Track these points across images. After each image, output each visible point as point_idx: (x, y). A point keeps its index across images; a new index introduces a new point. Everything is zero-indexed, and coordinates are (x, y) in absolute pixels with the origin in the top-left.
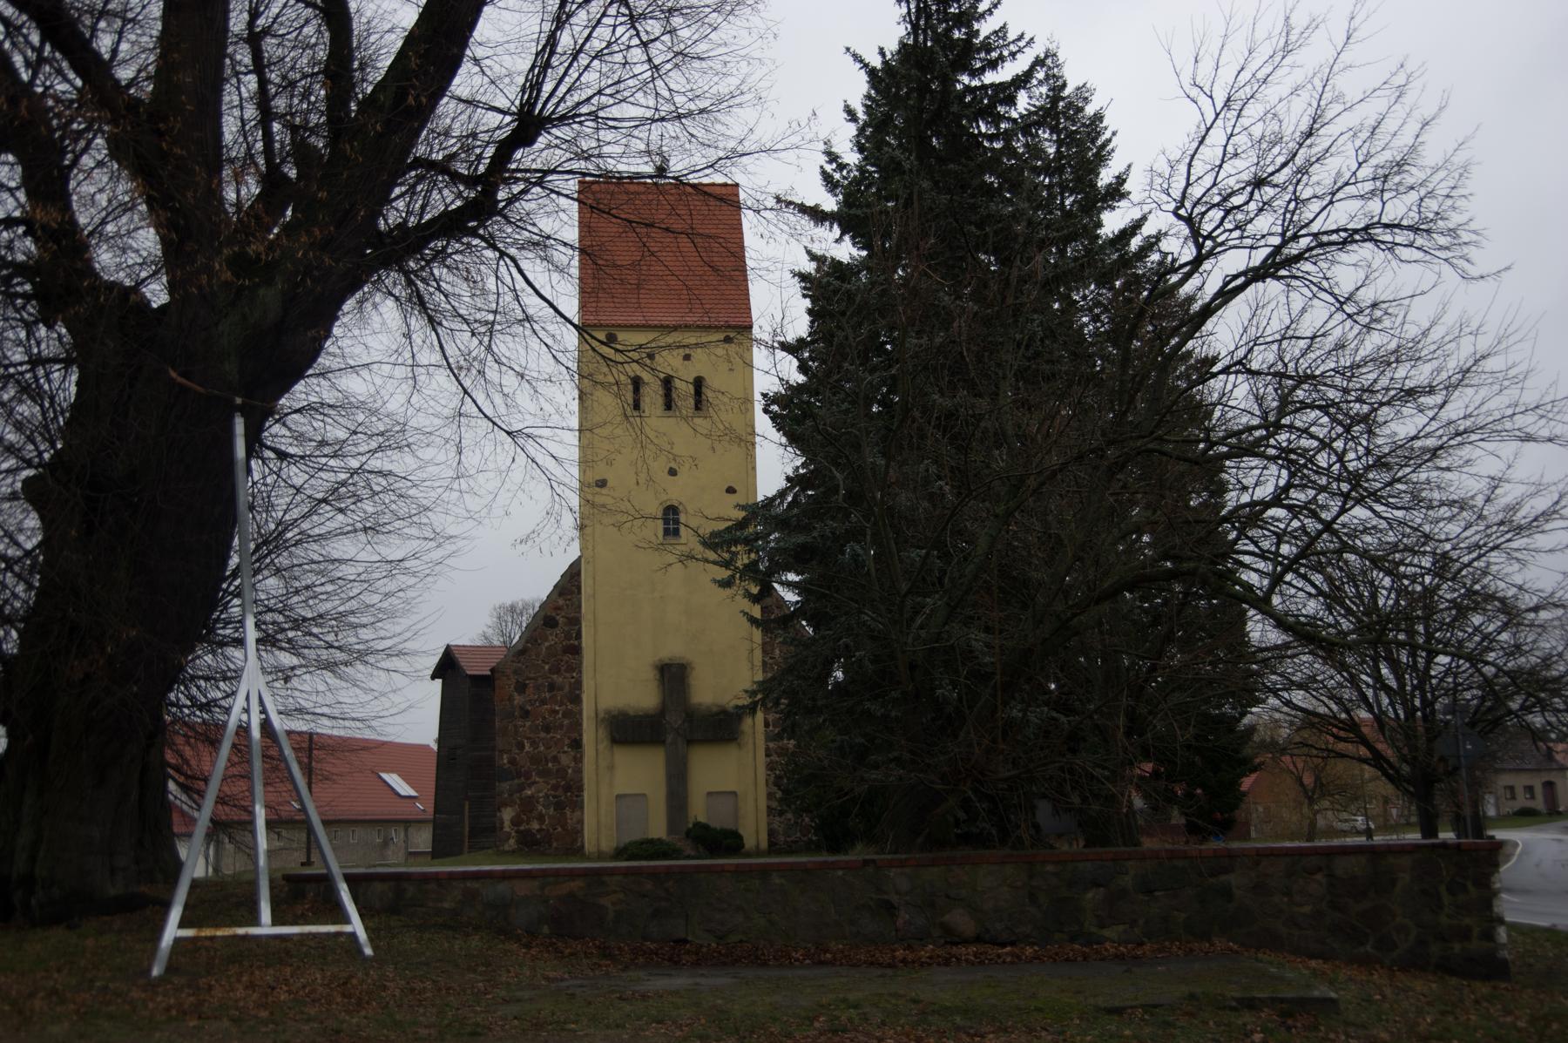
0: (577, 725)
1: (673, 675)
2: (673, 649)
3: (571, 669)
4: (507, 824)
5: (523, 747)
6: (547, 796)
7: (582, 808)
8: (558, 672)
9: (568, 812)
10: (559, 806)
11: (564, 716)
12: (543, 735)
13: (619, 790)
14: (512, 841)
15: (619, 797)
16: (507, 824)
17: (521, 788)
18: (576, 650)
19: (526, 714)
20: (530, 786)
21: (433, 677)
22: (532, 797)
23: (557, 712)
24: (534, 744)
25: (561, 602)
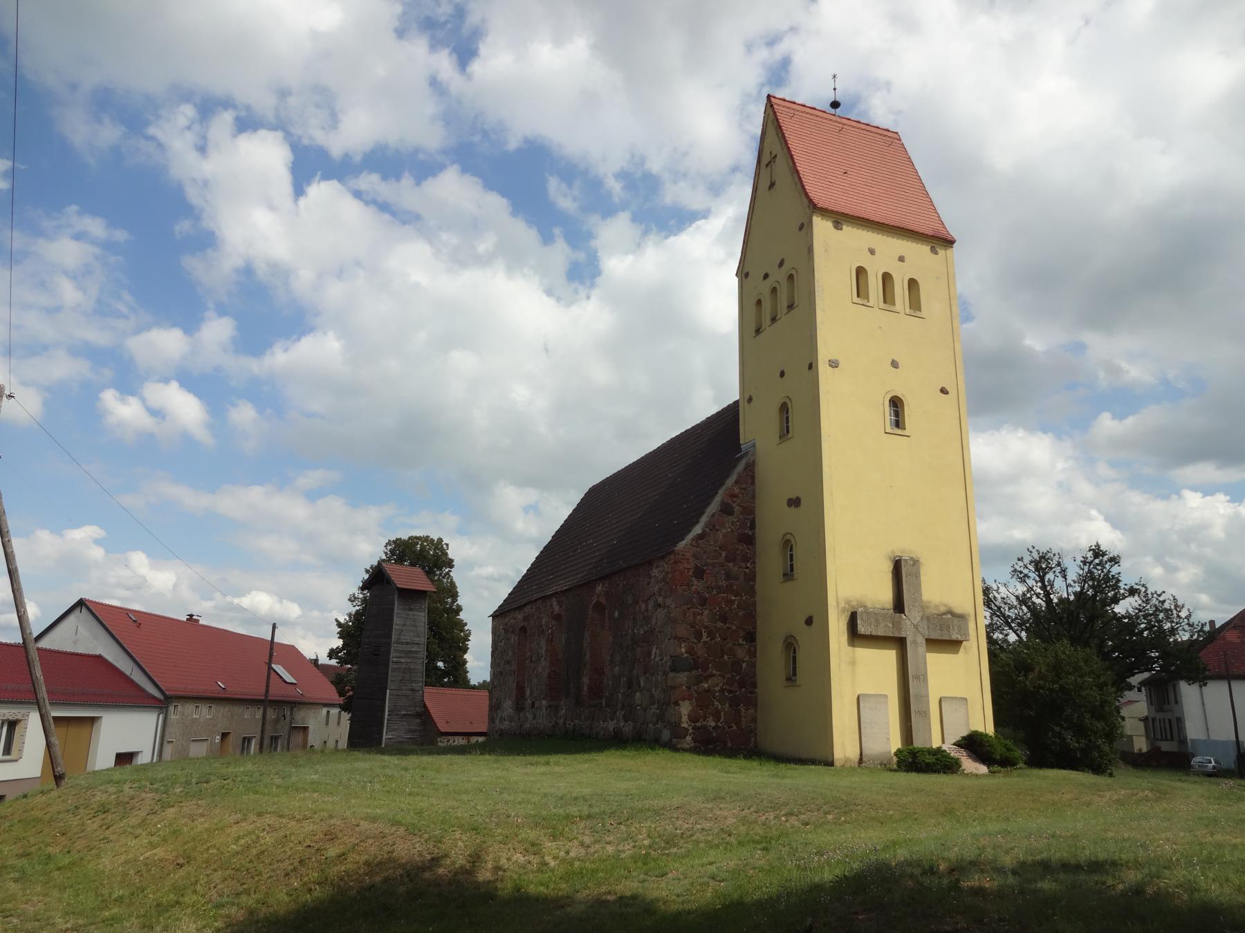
1: (901, 571)
2: (906, 545)
3: (746, 559)
4: (685, 718)
6: (722, 690)
9: (742, 708)
12: (720, 624)
14: (689, 738)
16: (685, 718)
17: (699, 680)
19: (704, 602)
20: (706, 679)
22: (708, 691)
23: (732, 602)
24: (710, 634)
25: (736, 490)
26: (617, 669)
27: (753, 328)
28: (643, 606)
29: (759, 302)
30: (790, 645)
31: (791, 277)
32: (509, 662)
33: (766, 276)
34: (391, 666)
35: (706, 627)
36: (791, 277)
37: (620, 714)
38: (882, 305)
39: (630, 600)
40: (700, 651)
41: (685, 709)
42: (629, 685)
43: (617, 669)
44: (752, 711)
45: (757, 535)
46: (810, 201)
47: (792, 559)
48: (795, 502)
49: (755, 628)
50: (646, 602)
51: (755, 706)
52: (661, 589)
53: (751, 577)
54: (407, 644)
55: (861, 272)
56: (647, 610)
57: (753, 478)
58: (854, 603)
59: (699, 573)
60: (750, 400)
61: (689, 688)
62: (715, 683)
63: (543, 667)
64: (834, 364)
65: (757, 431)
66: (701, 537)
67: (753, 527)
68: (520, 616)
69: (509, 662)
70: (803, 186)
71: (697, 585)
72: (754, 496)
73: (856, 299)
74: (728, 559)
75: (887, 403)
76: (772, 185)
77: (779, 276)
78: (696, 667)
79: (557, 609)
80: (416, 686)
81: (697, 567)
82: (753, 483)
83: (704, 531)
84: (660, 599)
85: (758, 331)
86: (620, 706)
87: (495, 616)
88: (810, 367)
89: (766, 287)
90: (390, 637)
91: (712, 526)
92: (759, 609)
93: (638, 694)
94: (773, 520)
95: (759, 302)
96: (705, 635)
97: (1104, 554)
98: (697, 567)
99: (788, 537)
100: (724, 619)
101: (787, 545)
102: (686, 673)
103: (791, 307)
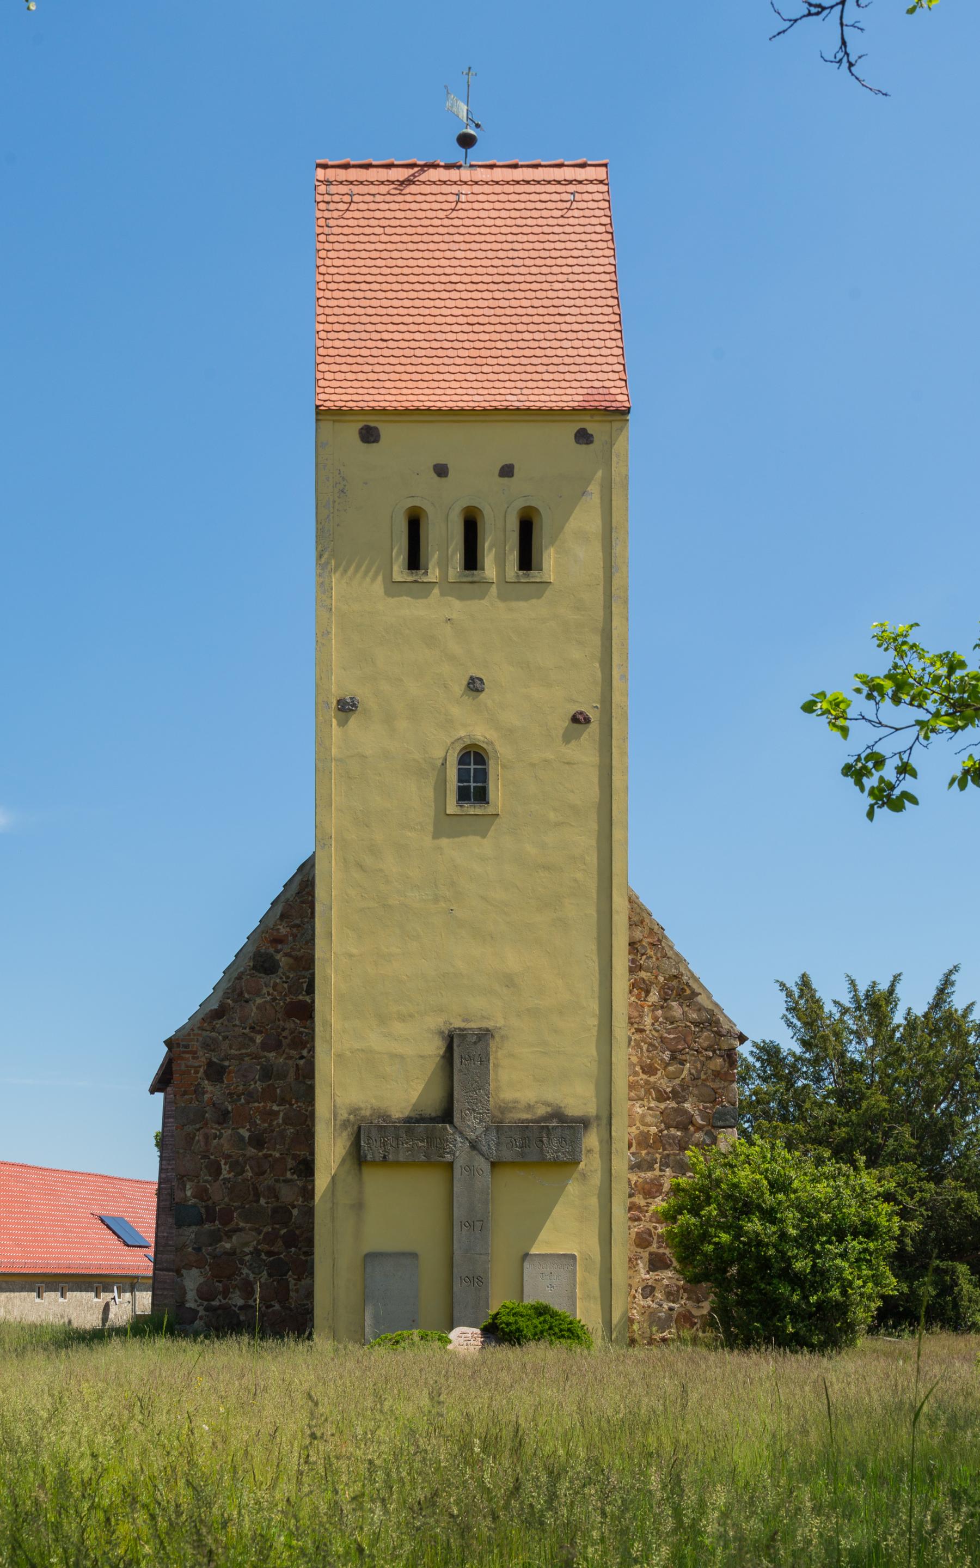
0: (307, 1136)
1: (463, 1051)
5: (218, 1171)
6: (257, 1252)
7: (312, 1274)
8: (277, 1046)
9: (291, 1278)
10: (278, 1269)
11: (287, 1120)
12: (251, 1151)
13: (368, 1248)
15: (371, 1258)
17: (215, 1238)
18: (305, 1012)
19: (223, 1117)
21: (153, 1090)
22: (232, 1253)
24: (237, 1167)
25: (283, 930)
35: (228, 1157)
40: (218, 1193)
59: (216, 1072)
61: (198, 1250)
62: (244, 1240)
67: (311, 990)
71: (211, 1091)
74: (265, 1046)
81: (210, 1064)
96: (225, 1169)
97: (633, 961)
100: (258, 1141)
102: (194, 1228)
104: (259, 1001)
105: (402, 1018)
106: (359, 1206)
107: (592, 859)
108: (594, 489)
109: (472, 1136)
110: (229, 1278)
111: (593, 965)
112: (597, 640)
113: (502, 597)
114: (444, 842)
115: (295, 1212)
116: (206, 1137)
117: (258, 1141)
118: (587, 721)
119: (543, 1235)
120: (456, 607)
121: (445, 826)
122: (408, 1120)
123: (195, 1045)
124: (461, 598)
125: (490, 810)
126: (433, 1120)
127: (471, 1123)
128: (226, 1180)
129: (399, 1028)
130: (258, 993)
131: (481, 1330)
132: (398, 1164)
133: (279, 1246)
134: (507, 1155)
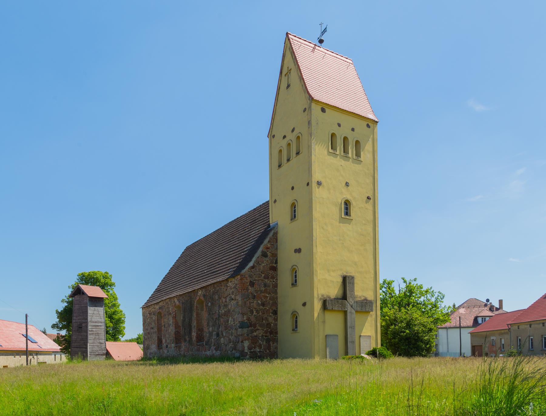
1: (346, 282)
2: (350, 271)
3: (273, 277)
4: (246, 348)
6: (262, 336)
8: (268, 278)
10: (268, 341)
12: (261, 307)
16: (246, 348)
17: (252, 332)
19: (254, 297)
22: (256, 336)
24: (257, 312)
25: (269, 245)
26: (211, 329)
27: (277, 164)
28: (224, 300)
29: (280, 151)
30: (295, 317)
31: (298, 138)
32: (152, 328)
33: (285, 137)
34: (89, 332)
36: (298, 138)
37: (213, 348)
38: (342, 153)
39: (217, 297)
40: (253, 319)
41: (246, 344)
42: (218, 335)
43: (211, 329)
44: (275, 344)
45: (278, 267)
46: (310, 96)
47: (296, 277)
48: (298, 251)
49: (277, 308)
50: (225, 298)
51: (277, 342)
52: (233, 292)
53: (276, 286)
54: (96, 322)
55: (333, 135)
56: (226, 302)
57: (277, 240)
58: (325, 296)
59: (252, 284)
60: (275, 201)
61: (248, 335)
62: (259, 333)
63: (172, 330)
64: (319, 184)
65: (279, 216)
66: (253, 267)
67: (276, 263)
68: (157, 307)
69: (152, 328)
70: (306, 87)
71: (251, 289)
72: (277, 249)
73: (331, 150)
74: (265, 278)
75: (343, 203)
76: (288, 86)
77: (291, 137)
78: (251, 326)
79: (177, 303)
80: (103, 341)
81: (251, 282)
82: (277, 242)
83: (254, 265)
84: (233, 296)
85: (280, 166)
86: (213, 344)
87: (145, 307)
88: (308, 184)
89: (284, 143)
90: (87, 319)
91: (258, 262)
92: (279, 300)
93: (222, 339)
94: (286, 259)
95: (280, 151)
96: (255, 312)
98: (251, 282)
99: (294, 267)
100: (263, 304)
101: (294, 272)
103: (298, 153)
104: (263, 265)
105: (334, 271)
106: (324, 322)
107: (372, 234)
108: (370, 140)
109: (351, 304)
110: (256, 343)
111: (372, 261)
112: (371, 178)
113: (353, 162)
114: (341, 224)
115: (272, 325)
116: (250, 303)
117: (263, 304)
118: (370, 199)
119: (364, 331)
120: (343, 162)
121: (342, 220)
122: (335, 299)
123: (247, 276)
124: (344, 160)
125: (351, 218)
126: (340, 299)
127: (350, 300)
128: (255, 315)
129: (332, 273)
130: (263, 262)
131: (157, 360)
132: (335, 311)
133: (268, 334)
134: (359, 309)
